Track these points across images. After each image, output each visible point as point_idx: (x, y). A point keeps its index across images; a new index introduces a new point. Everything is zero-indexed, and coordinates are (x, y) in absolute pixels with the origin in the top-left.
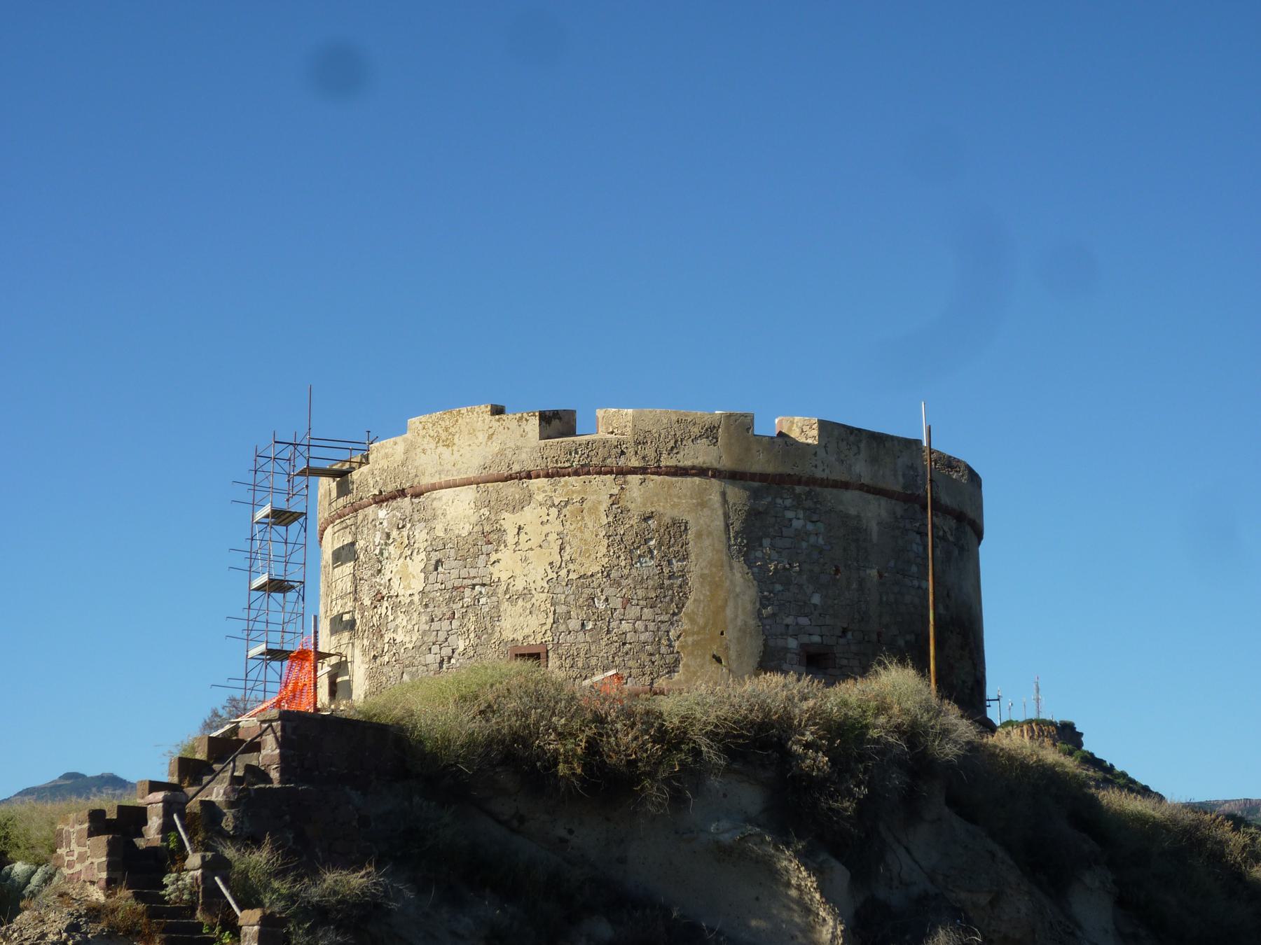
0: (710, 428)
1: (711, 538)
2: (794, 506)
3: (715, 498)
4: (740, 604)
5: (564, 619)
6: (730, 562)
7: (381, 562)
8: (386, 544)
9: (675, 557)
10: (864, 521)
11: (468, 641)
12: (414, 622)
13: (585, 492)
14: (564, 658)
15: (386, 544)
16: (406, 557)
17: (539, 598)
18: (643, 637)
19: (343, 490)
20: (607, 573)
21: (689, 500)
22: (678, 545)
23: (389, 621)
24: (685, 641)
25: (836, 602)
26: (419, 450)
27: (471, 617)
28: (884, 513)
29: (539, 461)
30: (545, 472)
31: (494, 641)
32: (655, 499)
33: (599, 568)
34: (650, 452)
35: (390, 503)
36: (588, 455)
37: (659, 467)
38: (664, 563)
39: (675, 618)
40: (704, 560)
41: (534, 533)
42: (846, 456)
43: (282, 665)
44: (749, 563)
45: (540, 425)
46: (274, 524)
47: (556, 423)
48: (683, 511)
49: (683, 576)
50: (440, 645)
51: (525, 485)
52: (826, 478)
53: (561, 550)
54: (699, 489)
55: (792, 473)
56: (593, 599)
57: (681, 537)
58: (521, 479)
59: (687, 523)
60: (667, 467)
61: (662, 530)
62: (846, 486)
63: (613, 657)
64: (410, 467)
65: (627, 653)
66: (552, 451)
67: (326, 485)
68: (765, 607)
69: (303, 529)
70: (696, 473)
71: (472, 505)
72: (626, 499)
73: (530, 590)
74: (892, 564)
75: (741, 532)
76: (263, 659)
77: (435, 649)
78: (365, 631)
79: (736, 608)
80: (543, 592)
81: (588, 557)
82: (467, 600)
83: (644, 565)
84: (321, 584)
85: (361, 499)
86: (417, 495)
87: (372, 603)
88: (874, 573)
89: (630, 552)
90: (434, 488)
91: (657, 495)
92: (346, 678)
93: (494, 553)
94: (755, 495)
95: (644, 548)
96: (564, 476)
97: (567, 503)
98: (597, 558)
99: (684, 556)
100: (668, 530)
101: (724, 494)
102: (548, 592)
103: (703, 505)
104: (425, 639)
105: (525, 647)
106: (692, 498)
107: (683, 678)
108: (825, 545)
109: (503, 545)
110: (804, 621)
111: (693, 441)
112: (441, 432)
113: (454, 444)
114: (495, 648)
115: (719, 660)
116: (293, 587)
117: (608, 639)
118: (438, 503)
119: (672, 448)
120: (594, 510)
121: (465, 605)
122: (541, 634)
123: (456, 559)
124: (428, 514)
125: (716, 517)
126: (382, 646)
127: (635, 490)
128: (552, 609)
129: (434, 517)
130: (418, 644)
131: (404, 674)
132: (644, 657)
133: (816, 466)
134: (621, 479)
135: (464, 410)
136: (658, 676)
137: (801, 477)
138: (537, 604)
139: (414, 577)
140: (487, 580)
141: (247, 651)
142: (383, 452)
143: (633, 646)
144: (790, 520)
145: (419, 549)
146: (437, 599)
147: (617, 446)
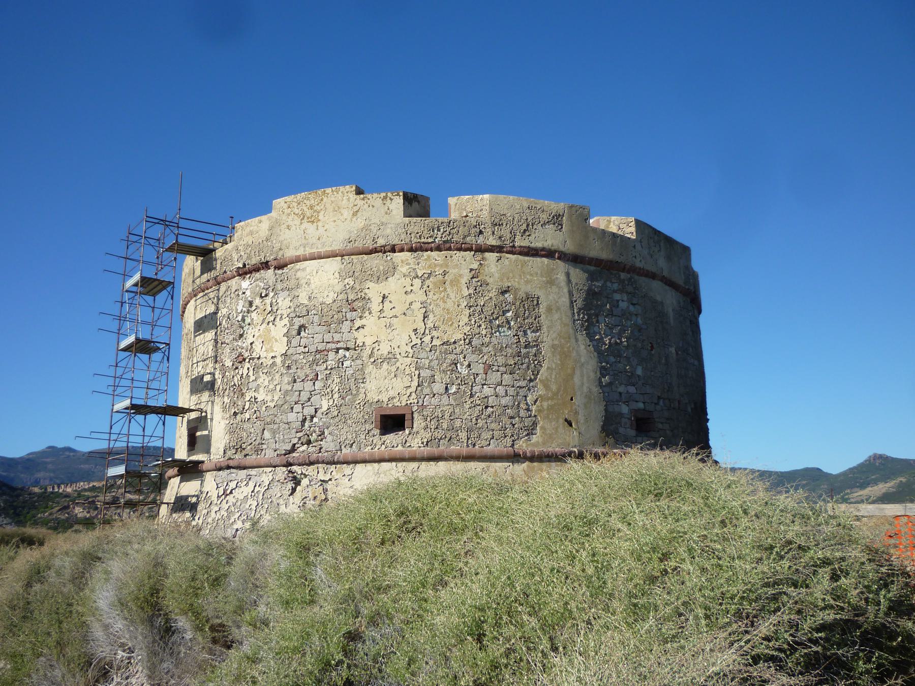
3: (561, 277)
4: (585, 373)
5: (429, 383)
7: (243, 328)
8: (248, 312)
9: (529, 328)
11: (331, 401)
13: (447, 266)
15: (248, 312)
16: (269, 322)
17: (403, 362)
18: (504, 401)
19: (207, 267)
21: (540, 278)
22: (532, 318)
23: (251, 380)
24: (541, 405)
25: (652, 373)
26: (285, 226)
27: (335, 379)
29: (403, 237)
31: (359, 401)
34: (505, 232)
35: (253, 274)
36: (450, 232)
37: (514, 246)
38: (521, 334)
39: (531, 384)
40: (554, 332)
41: (398, 301)
42: (653, 252)
43: (154, 300)
44: (590, 336)
45: (404, 204)
46: (141, 293)
47: (415, 204)
48: (535, 287)
49: (537, 345)
50: (302, 404)
51: (389, 258)
53: (424, 317)
54: (548, 269)
55: (619, 261)
56: (456, 364)
59: (538, 298)
60: (521, 247)
61: (518, 303)
62: (653, 276)
63: (477, 420)
64: (274, 242)
65: (489, 416)
67: (191, 263)
69: (170, 297)
71: (337, 275)
72: (485, 274)
73: (394, 355)
75: (582, 309)
76: (128, 413)
77: (298, 408)
78: (226, 389)
79: (582, 376)
80: (407, 356)
81: (451, 325)
82: (331, 363)
83: (502, 334)
84: (183, 350)
85: (225, 272)
87: (233, 365)
88: (673, 350)
90: (298, 260)
92: (206, 433)
93: (359, 319)
94: (592, 277)
95: (502, 319)
96: (427, 251)
98: (459, 326)
100: (523, 303)
101: (568, 275)
102: (412, 357)
103: (551, 282)
104: (288, 398)
105: (390, 408)
106: (542, 276)
107: (540, 440)
109: (367, 312)
110: (632, 389)
111: (542, 226)
112: (305, 209)
114: (360, 408)
116: (159, 349)
117: (471, 403)
118: (302, 273)
119: (525, 231)
120: (455, 282)
121: (329, 368)
123: (320, 325)
124: (292, 283)
126: (243, 404)
127: (492, 266)
128: (417, 373)
129: (298, 286)
130: (280, 403)
131: (265, 431)
132: (505, 419)
134: (479, 256)
135: (329, 190)
136: (518, 438)
137: (625, 265)
139: (276, 341)
140: (351, 345)
141: (113, 405)
142: (248, 230)
143: (495, 409)
145: (282, 315)
146: (300, 361)
147: (475, 226)
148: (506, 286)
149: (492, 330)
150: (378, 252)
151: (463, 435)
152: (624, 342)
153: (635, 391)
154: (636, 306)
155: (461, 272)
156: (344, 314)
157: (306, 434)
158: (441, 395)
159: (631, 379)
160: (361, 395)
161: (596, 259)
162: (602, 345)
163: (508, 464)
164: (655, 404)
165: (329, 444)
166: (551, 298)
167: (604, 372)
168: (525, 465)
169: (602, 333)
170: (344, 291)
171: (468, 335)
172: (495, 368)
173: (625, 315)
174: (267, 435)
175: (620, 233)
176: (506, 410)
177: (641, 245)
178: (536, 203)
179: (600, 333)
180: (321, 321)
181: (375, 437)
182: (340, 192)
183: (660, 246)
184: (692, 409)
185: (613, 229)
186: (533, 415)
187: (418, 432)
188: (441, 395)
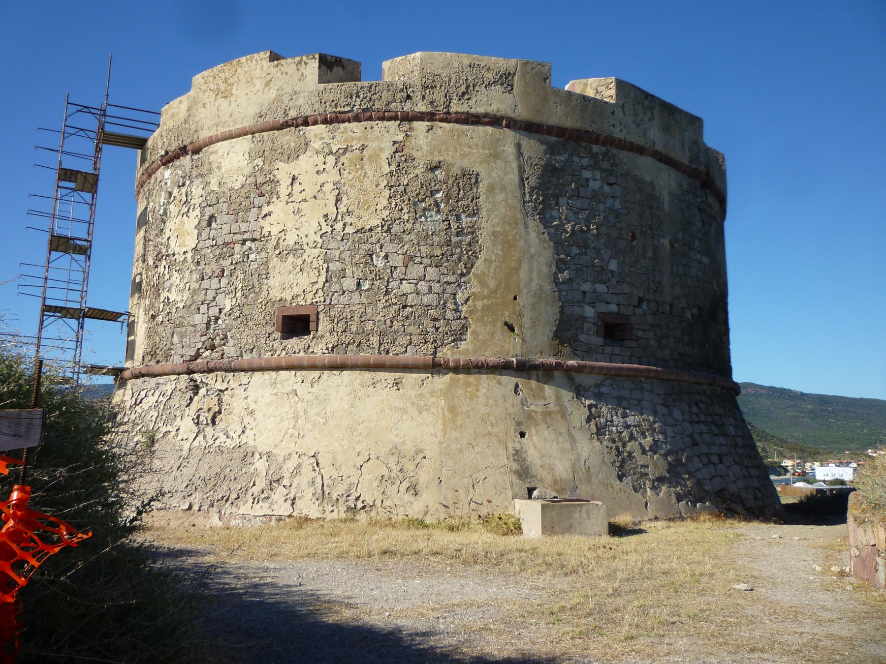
0: (505, 74)
1: (504, 193)
2: (591, 166)
3: (510, 150)
4: (535, 266)
6: (524, 219)
8: (169, 203)
9: (464, 212)
10: (658, 189)
11: (234, 300)
12: (186, 281)
13: (366, 139)
14: (336, 321)
18: (426, 300)
20: (388, 227)
21: (481, 151)
22: (468, 199)
24: (474, 305)
25: (633, 269)
26: (200, 105)
28: (673, 184)
29: (317, 106)
30: (323, 117)
31: (261, 300)
32: (444, 147)
33: (379, 222)
34: (439, 96)
36: (370, 99)
37: (448, 113)
38: (452, 218)
39: (463, 279)
40: (496, 216)
41: (309, 182)
42: (642, 120)
44: (545, 222)
45: (319, 68)
49: (473, 233)
50: (208, 304)
51: (301, 133)
52: (623, 138)
53: (337, 201)
54: (492, 140)
55: (590, 130)
56: (371, 255)
57: (471, 189)
58: (297, 126)
59: (478, 175)
60: (457, 113)
61: (450, 182)
62: (641, 150)
63: (392, 322)
65: (407, 318)
66: (331, 95)
68: (561, 271)
70: (489, 121)
71: (247, 156)
72: (411, 146)
74: (680, 236)
79: (531, 270)
80: (316, 247)
83: (429, 219)
86: (197, 151)
87: (154, 263)
88: (666, 242)
89: (413, 205)
90: (211, 142)
91: (445, 143)
94: (552, 149)
95: (430, 201)
96: (344, 122)
97: (346, 150)
98: (376, 210)
99: (474, 211)
101: (518, 146)
102: (321, 247)
103: (496, 156)
106: (484, 148)
107: (470, 347)
108: (622, 208)
110: (601, 288)
111: (486, 87)
112: (220, 83)
113: (232, 94)
115: (512, 329)
117: (386, 301)
119: (463, 94)
120: (375, 157)
121: (234, 262)
122: (312, 293)
125: (510, 170)
127: (421, 137)
128: (325, 266)
129: (210, 171)
130: (188, 303)
132: (428, 323)
133: (614, 126)
134: (406, 125)
136: (442, 345)
137: (599, 135)
138: (309, 260)
139: (189, 234)
140: (257, 235)
143: (414, 309)
144: (587, 180)
148: (437, 160)
149: (416, 214)
150: (290, 126)
151: (375, 340)
152: (593, 229)
153: (606, 290)
154: (614, 186)
155: (383, 145)
156: (252, 200)
157: (210, 338)
158: (352, 292)
159: (601, 275)
160: (263, 293)
161: (558, 128)
162: (562, 233)
163: (426, 375)
164: (635, 307)
165: (230, 350)
166: (494, 174)
167: (563, 266)
168: (447, 377)
169: (563, 217)
170: (253, 174)
171: (387, 221)
172: (418, 260)
173: (597, 197)
174: (176, 339)
175: (598, 97)
176: (428, 310)
177: (624, 111)
178: (479, 60)
179: (560, 218)
180: (229, 209)
181: (276, 341)
182: (254, 61)
183: (652, 114)
184: (693, 315)
185: (590, 93)
186: (462, 317)
187: (322, 336)
188: (352, 292)
